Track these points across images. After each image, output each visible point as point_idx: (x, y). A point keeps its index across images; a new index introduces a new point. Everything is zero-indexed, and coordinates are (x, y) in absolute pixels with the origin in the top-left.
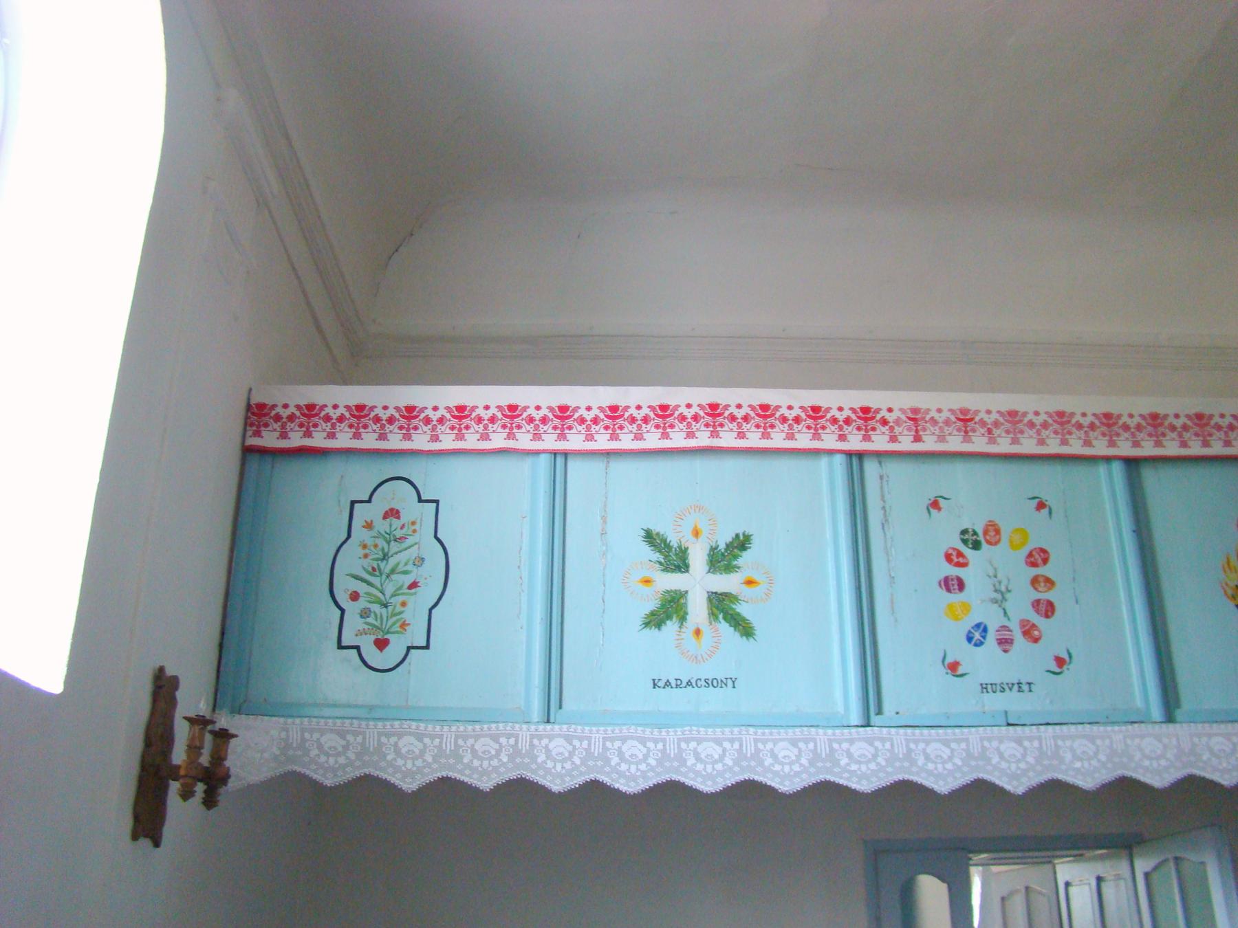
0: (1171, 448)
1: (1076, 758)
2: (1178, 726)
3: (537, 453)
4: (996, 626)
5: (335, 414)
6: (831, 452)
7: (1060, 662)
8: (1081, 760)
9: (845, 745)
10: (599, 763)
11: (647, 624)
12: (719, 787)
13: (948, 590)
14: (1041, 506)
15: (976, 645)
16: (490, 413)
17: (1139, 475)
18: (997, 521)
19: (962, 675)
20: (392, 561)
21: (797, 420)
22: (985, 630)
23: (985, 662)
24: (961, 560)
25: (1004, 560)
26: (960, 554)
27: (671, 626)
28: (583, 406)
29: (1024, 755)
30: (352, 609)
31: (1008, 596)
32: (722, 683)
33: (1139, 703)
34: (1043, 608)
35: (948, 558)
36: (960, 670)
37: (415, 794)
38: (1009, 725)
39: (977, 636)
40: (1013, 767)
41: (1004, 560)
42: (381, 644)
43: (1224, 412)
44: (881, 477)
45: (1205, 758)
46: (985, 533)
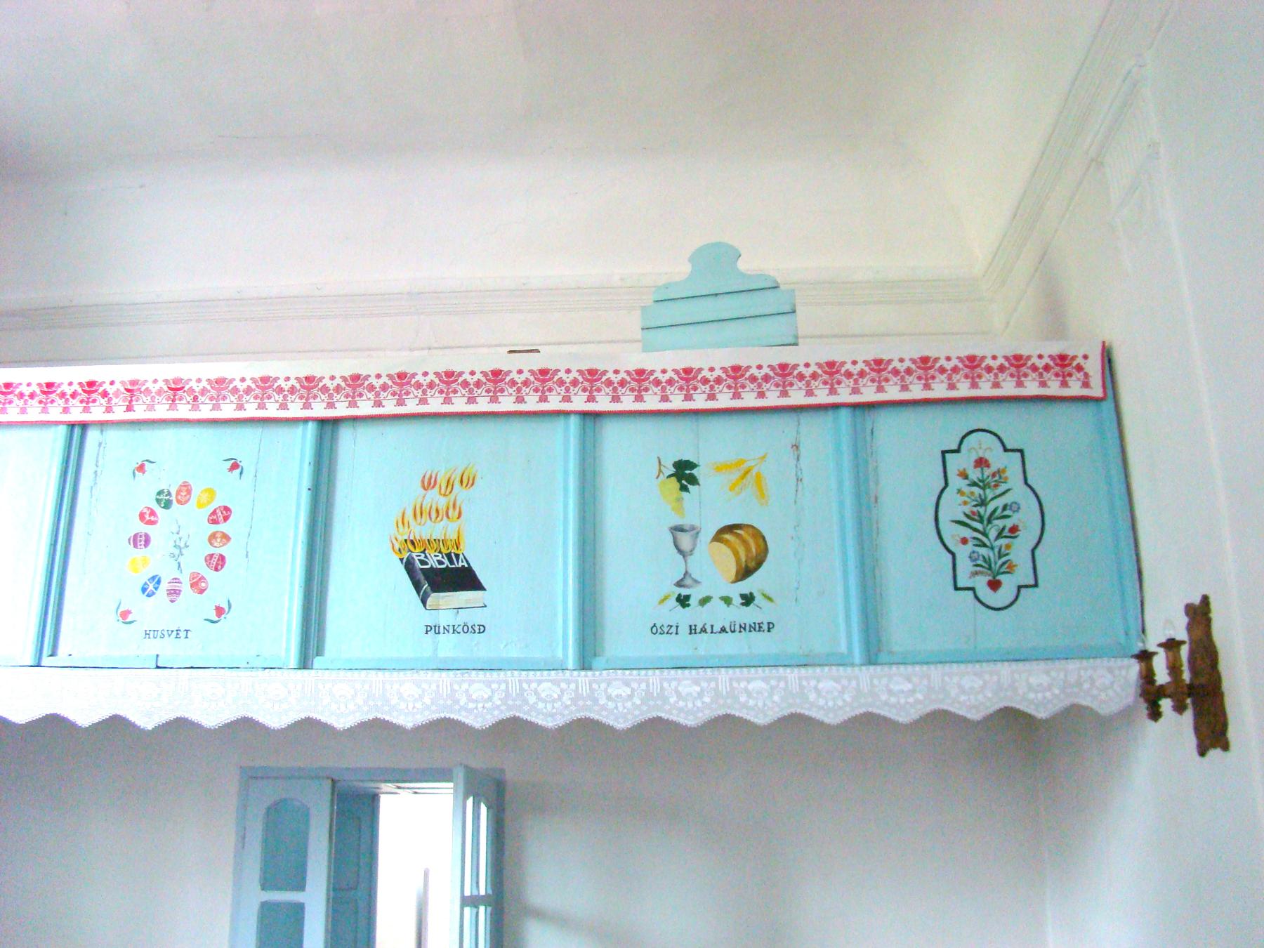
0: (365, 407)
2: (879, 668)
3: (567, 413)
4: (169, 579)
5: (287, 386)
6: (57, 423)
7: (220, 611)
8: (1037, 692)
9: (884, 681)
10: (729, 701)
13: (135, 545)
14: (141, 468)
15: (148, 596)
16: (428, 379)
17: (334, 439)
18: (191, 482)
20: (991, 507)
21: (862, 374)
22: (159, 582)
23: (155, 612)
24: (152, 518)
25: (189, 521)
26: (153, 513)
28: (468, 371)
31: (184, 551)
33: (843, 648)
34: (214, 561)
35: (142, 516)
39: (151, 587)
41: (189, 521)
42: (994, 585)
43: (904, 356)
44: (100, 444)
45: (672, 700)
46: (178, 493)
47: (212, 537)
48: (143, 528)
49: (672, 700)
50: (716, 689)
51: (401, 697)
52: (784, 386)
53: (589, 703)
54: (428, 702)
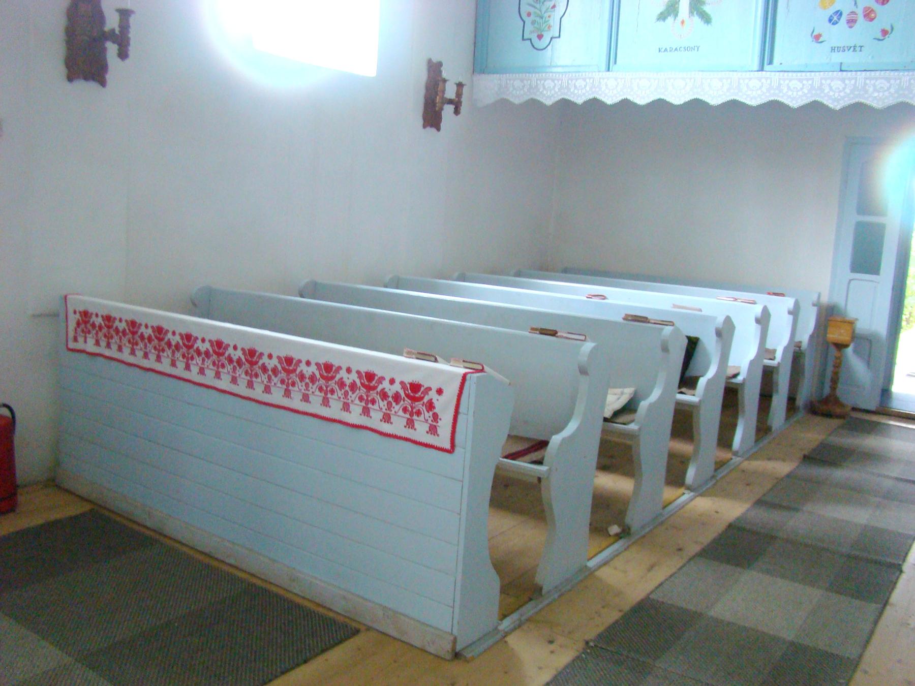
1: (875, 90)
7: (885, 33)
8: (879, 92)
9: (746, 81)
11: (658, 19)
12: (682, 102)
19: (892, 29)
22: (841, 14)
23: (839, 34)
27: (670, 20)
29: (844, 89)
30: (528, 21)
32: (692, 49)
36: (888, 28)
37: (552, 106)
38: (841, 71)
39: (835, 18)
40: (836, 95)
49: (785, 91)
50: (812, 85)
53: (862, 93)
54: (806, 91)
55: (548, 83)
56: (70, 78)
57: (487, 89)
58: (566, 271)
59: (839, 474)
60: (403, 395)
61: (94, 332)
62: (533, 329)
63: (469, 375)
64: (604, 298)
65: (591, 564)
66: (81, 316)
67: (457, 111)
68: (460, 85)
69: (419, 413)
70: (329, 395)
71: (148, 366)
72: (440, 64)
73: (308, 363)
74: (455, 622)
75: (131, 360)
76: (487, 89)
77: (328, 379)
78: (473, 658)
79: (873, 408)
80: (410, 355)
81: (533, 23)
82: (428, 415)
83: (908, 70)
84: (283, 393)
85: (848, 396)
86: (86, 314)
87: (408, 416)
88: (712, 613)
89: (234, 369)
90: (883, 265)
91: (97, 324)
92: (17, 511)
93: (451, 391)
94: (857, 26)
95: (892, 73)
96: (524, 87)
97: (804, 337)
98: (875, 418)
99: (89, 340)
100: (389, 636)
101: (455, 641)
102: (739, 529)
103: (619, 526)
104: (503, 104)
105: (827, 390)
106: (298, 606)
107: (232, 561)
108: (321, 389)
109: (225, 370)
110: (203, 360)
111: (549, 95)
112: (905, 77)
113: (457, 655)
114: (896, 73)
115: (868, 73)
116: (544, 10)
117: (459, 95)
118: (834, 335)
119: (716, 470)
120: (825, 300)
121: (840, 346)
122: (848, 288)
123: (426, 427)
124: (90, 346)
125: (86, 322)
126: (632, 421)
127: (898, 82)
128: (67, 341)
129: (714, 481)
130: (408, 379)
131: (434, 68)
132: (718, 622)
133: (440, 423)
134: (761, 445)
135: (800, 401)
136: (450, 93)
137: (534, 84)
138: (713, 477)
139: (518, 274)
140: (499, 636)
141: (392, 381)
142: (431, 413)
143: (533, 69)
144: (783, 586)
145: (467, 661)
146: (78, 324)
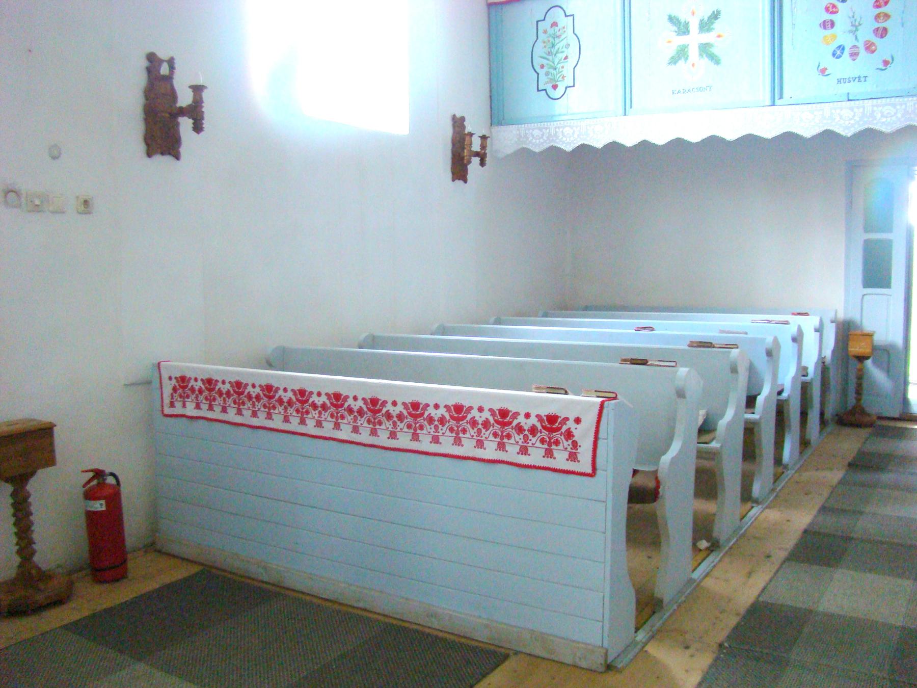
1: (882, 116)
7: (886, 63)
9: (838, 111)
20: (556, 47)
22: (843, 49)
23: (844, 67)
27: (681, 63)
30: (542, 72)
34: (880, 32)
35: (827, 9)
36: (889, 59)
37: (541, 153)
38: (849, 100)
39: (838, 52)
47: (877, 17)
48: (829, 17)
51: (841, 118)
52: (550, 444)
55: (567, 130)
56: (149, 155)
57: (506, 140)
58: (586, 308)
59: (885, 477)
60: (539, 427)
61: (193, 396)
62: (624, 361)
63: (606, 403)
64: (651, 329)
65: (696, 575)
66: (178, 381)
67: (482, 163)
68: (484, 138)
69: (557, 443)
70: (461, 435)
71: (258, 424)
72: (463, 119)
73: (437, 406)
74: (605, 635)
75: (238, 419)
76: (506, 140)
77: (458, 420)
78: (624, 668)
79: (896, 415)
80: (539, 389)
81: (547, 74)
82: (567, 444)
83: (912, 96)
84: (410, 437)
85: (874, 406)
86: (183, 379)
87: (546, 446)
88: (821, 609)
89: (355, 420)
90: (893, 281)
91: (197, 388)
92: (130, 576)
93: (589, 420)
94: (859, 58)
95: (897, 99)
96: (543, 135)
97: (828, 353)
98: (900, 424)
99: (188, 404)
100: (538, 657)
101: (606, 654)
102: (815, 533)
103: (708, 541)
104: (524, 154)
105: (851, 401)
106: (443, 640)
107: (361, 605)
108: (451, 430)
109: (345, 421)
110: (320, 413)
111: (568, 142)
112: (910, 102)
113: (609, 667)
114: (901, 99)
115: (875, 101)
116: (556, 61)
117: (483, 147)
118: (856, 348)
119: (775, 482)
120: (841, 316)
121: (861, 359)
122: (862, 303)
123: (566, 455)
124: (190, 410)
125: (184, 388)
126: (713, 440)
127: (903, 107)
128: (162, 406)
129: (775, 494)
130: (544, 412)
131: (458, 123)
132: (830, 616)
133: (580, 450)
134: (805, 457)
135: (828, 416)
136: (476, 146)
137: (553, 132)
138: (773, 490)
139: (546, 315)
140: (639, 647)
141: (224, 382)
142: (570, 442)
143: (550, 118)
144: (871, 579)
145: (619, 671)
146: (175, 389)
